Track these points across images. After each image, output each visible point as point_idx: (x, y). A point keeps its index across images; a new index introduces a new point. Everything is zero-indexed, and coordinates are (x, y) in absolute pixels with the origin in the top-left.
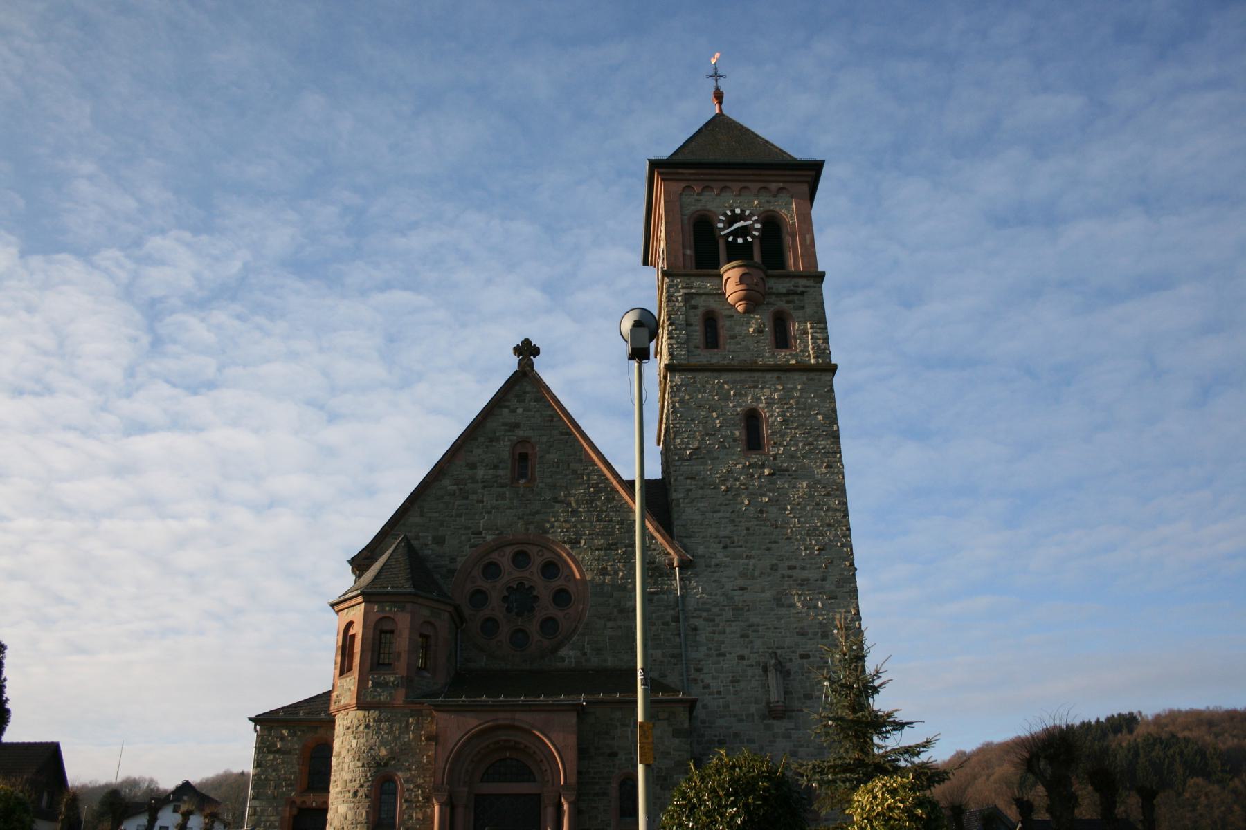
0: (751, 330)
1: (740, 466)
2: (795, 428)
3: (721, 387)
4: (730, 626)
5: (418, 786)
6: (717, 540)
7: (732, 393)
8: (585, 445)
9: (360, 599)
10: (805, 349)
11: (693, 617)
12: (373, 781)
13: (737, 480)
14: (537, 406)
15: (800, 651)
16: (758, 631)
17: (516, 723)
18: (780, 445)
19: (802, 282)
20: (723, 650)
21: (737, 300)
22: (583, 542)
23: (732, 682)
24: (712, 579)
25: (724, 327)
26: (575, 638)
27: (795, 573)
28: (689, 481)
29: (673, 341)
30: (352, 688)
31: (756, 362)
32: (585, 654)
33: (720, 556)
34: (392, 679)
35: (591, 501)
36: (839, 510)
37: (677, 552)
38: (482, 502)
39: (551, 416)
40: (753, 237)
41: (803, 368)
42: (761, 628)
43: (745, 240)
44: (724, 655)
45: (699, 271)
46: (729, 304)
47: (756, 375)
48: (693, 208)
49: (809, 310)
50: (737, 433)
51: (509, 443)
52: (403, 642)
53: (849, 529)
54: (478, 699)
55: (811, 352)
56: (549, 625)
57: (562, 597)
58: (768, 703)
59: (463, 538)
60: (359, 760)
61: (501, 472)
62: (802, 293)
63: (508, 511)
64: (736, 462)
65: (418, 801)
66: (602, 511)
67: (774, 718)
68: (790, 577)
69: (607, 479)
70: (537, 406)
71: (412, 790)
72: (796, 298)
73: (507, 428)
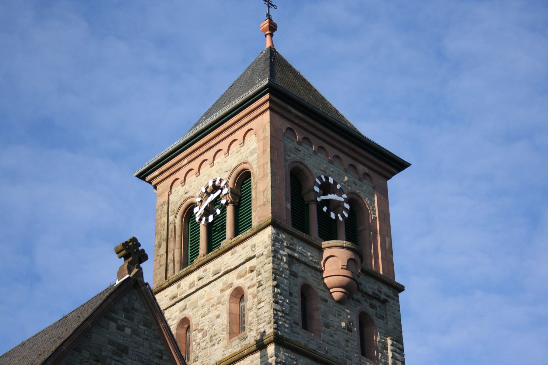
0: (343, 324)
14: (147, 333)
19: (385, 289)
21: (336, 286)
39: (160, 351)
40: (343, 216)
46: (325, 284)
62: (384, 302)
70: (147, 333)
72: (377, 304)
73: (114, 348)
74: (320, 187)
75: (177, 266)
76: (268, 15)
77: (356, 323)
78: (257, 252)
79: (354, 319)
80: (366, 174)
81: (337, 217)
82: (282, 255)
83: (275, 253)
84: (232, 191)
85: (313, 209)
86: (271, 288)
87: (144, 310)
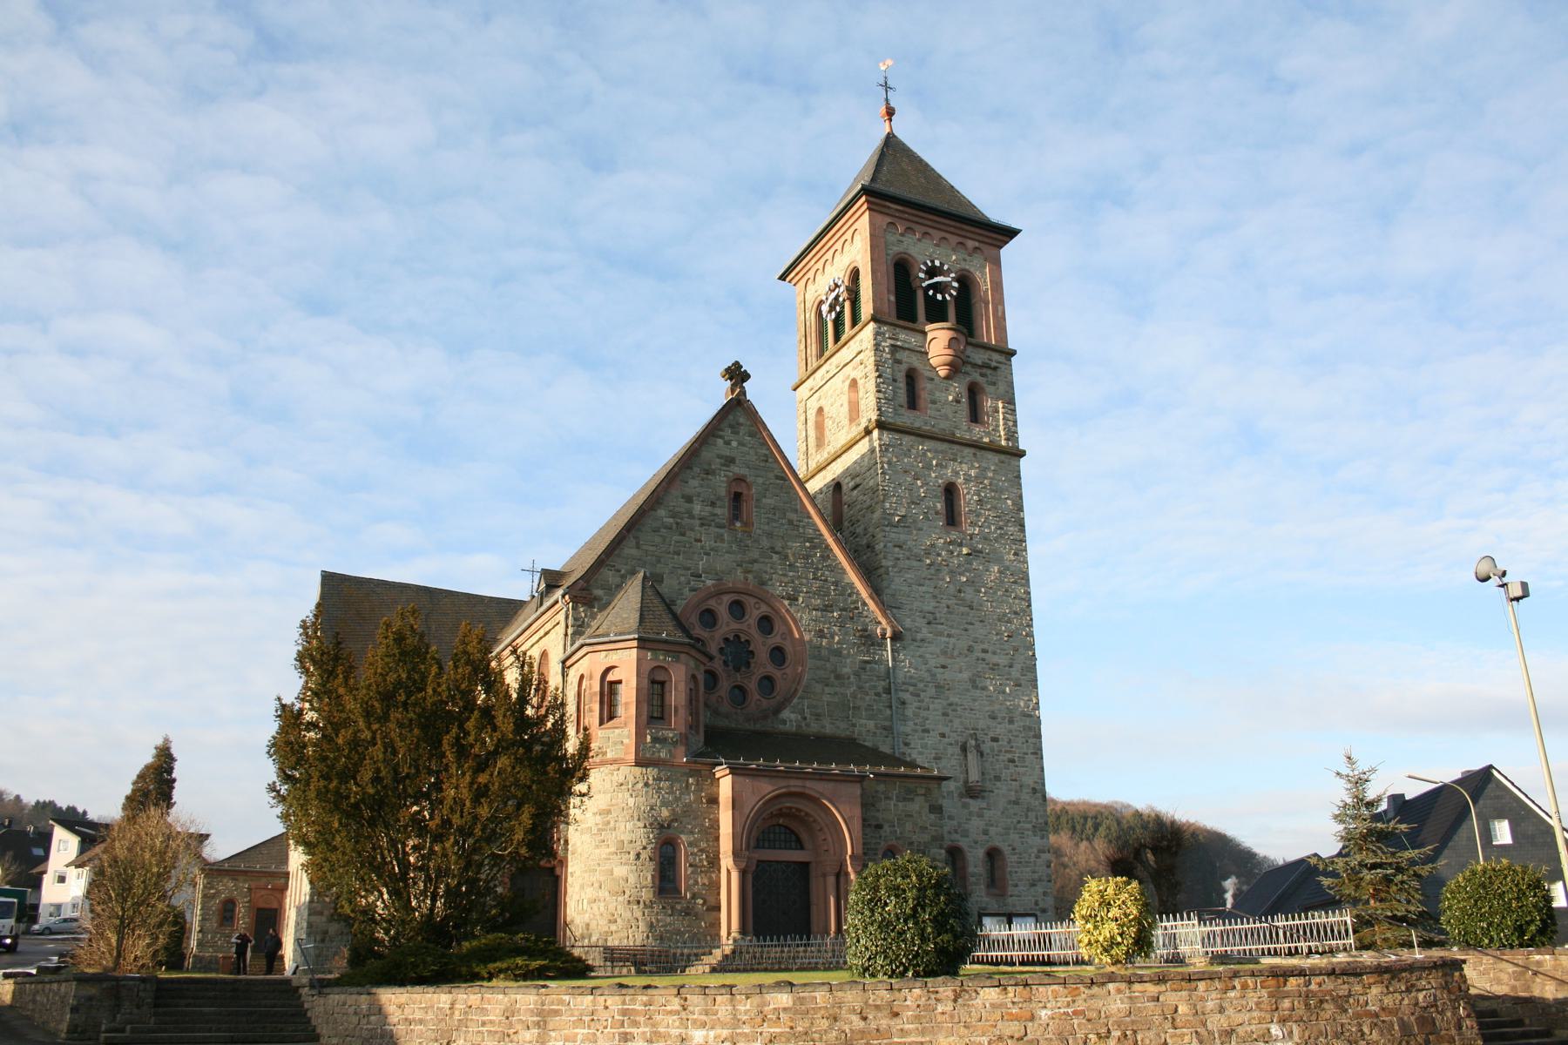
0: (951, 398)
1: (942, 541)
2: (989, 510)
3: (924, 454)
4: (933, 703)
5: (702, 851)
6: (922, 614)
7: (934, 462)
8: (801, 494)
9: (635, 643)
10: (996, 429)
11: (902, 690)
12: (656, 843)
13: (939, 555)
15: (991, 734)
16: (956, 711)
17: (807, 791)
18: (976, 525)
19: (996, 356)
20: (927, 726)
22: (801, 600)
23: (935, 758)
24: (918, 654)
25: (925, 390)
26: (795, 701)
27: (988, 656)
28: (897, 549)
29: (881, 395)
30: (626, 741)
31: (954, 434)
32: (805, 718)
33: (924, 630)
34: (671, 735)
35: (807, 557)
36: (1024, 599)
37: (889, 622)
38: (700, 541)
39: (766, 455)
40: (951, 295)
41: (1000, 451)
42: (959, 708)
43: (944, 297)
44: (927, 731)
45: (901, 323)
47: (956, 447)
48: (896, 249)
49: (1002, 387)
50: (939, 505)
51: (725, 479)
52: (677, 696)
53: (1031, 620)
54: (772, 764)
55: (1002, 433)
56: (768, 683)
57: (778, 654)
58: (966, 782)
59: (682, 579)
60: (639, 820)
61: (718, 511)
62: (995, 369)
63: (727, 555)
64: (937, 536)
65: (703, 866)
66: (817, 569)
67: (971, 797)
68: (983, 660)
69: (821, 535)
71: (696, 855)
72: (989, 372)
73: (723, 461)
74: (926, 273)
75: (814, 359)
76: (887, 100)
77: (965, 394)
78: (863, 348)
79: (962, 391)
80: (976, 248)
81: (944, 297)
82: (884, 347)
83: (877, 347)
84: (847, 289)
85: (920, 294)
86: (874, 380)
87: (748, 423)
